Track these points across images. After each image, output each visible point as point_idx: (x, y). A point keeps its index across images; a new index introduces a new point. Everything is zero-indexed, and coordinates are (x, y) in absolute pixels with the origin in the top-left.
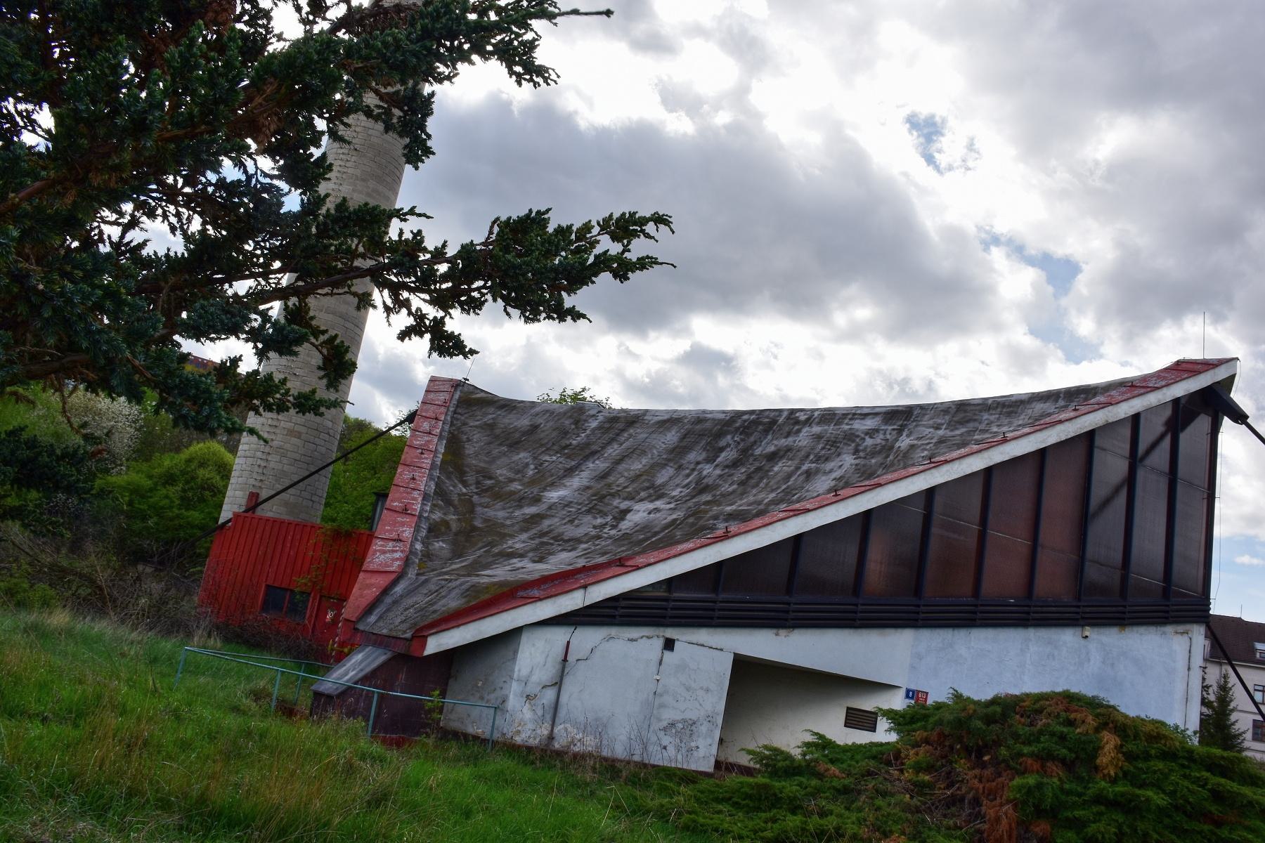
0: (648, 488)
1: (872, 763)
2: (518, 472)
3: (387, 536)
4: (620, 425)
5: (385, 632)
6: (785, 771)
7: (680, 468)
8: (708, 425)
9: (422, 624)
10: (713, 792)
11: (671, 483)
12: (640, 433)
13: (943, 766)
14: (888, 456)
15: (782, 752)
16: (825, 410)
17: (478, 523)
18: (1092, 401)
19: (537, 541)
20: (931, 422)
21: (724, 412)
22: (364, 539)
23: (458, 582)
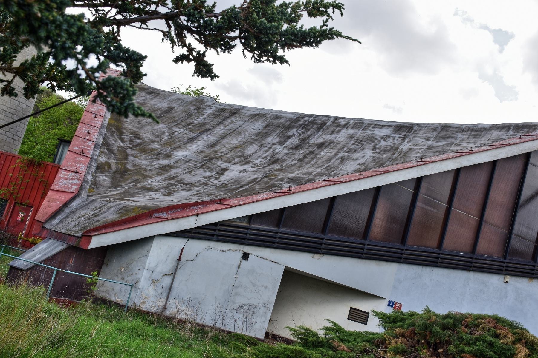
0: (240, 156)
1: (368, 344)
2: (158, 136)
3: (69, 168)
4: (226, 114)
5: (63, 231)
6: (313, 344)
7: (262, 146)
8: (282, 121)
9: (89, 228)
10: (267, 352)
11: (255, 155)
12: (237, 121)
13: (412, 352)
14: (394, 154)
15: (312, 332)
16: (357, 119)
17: (129, 166)
18: (532, 134)
19: (167, 182)
20: (424, 135)
21: (293, 113)
22: (50, 168)
23: (115, 204)
